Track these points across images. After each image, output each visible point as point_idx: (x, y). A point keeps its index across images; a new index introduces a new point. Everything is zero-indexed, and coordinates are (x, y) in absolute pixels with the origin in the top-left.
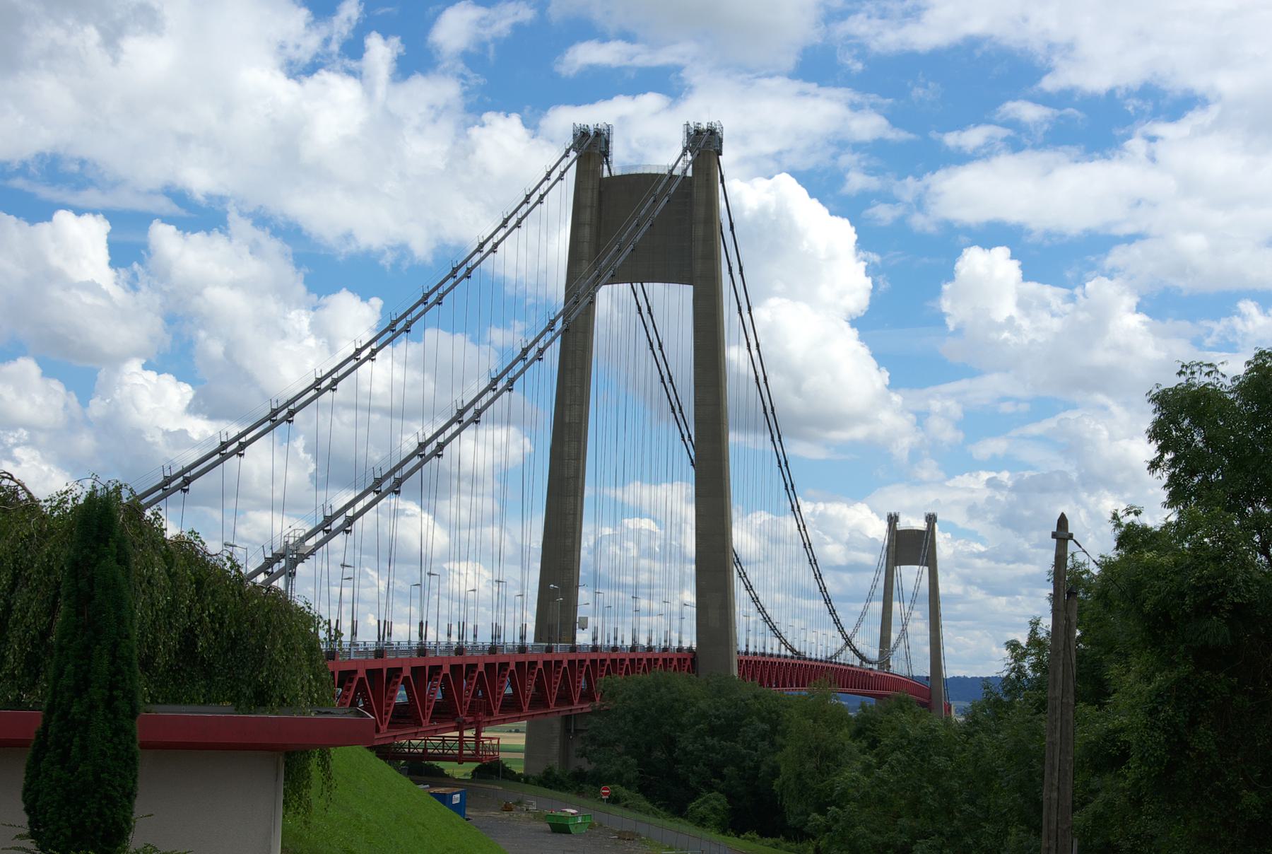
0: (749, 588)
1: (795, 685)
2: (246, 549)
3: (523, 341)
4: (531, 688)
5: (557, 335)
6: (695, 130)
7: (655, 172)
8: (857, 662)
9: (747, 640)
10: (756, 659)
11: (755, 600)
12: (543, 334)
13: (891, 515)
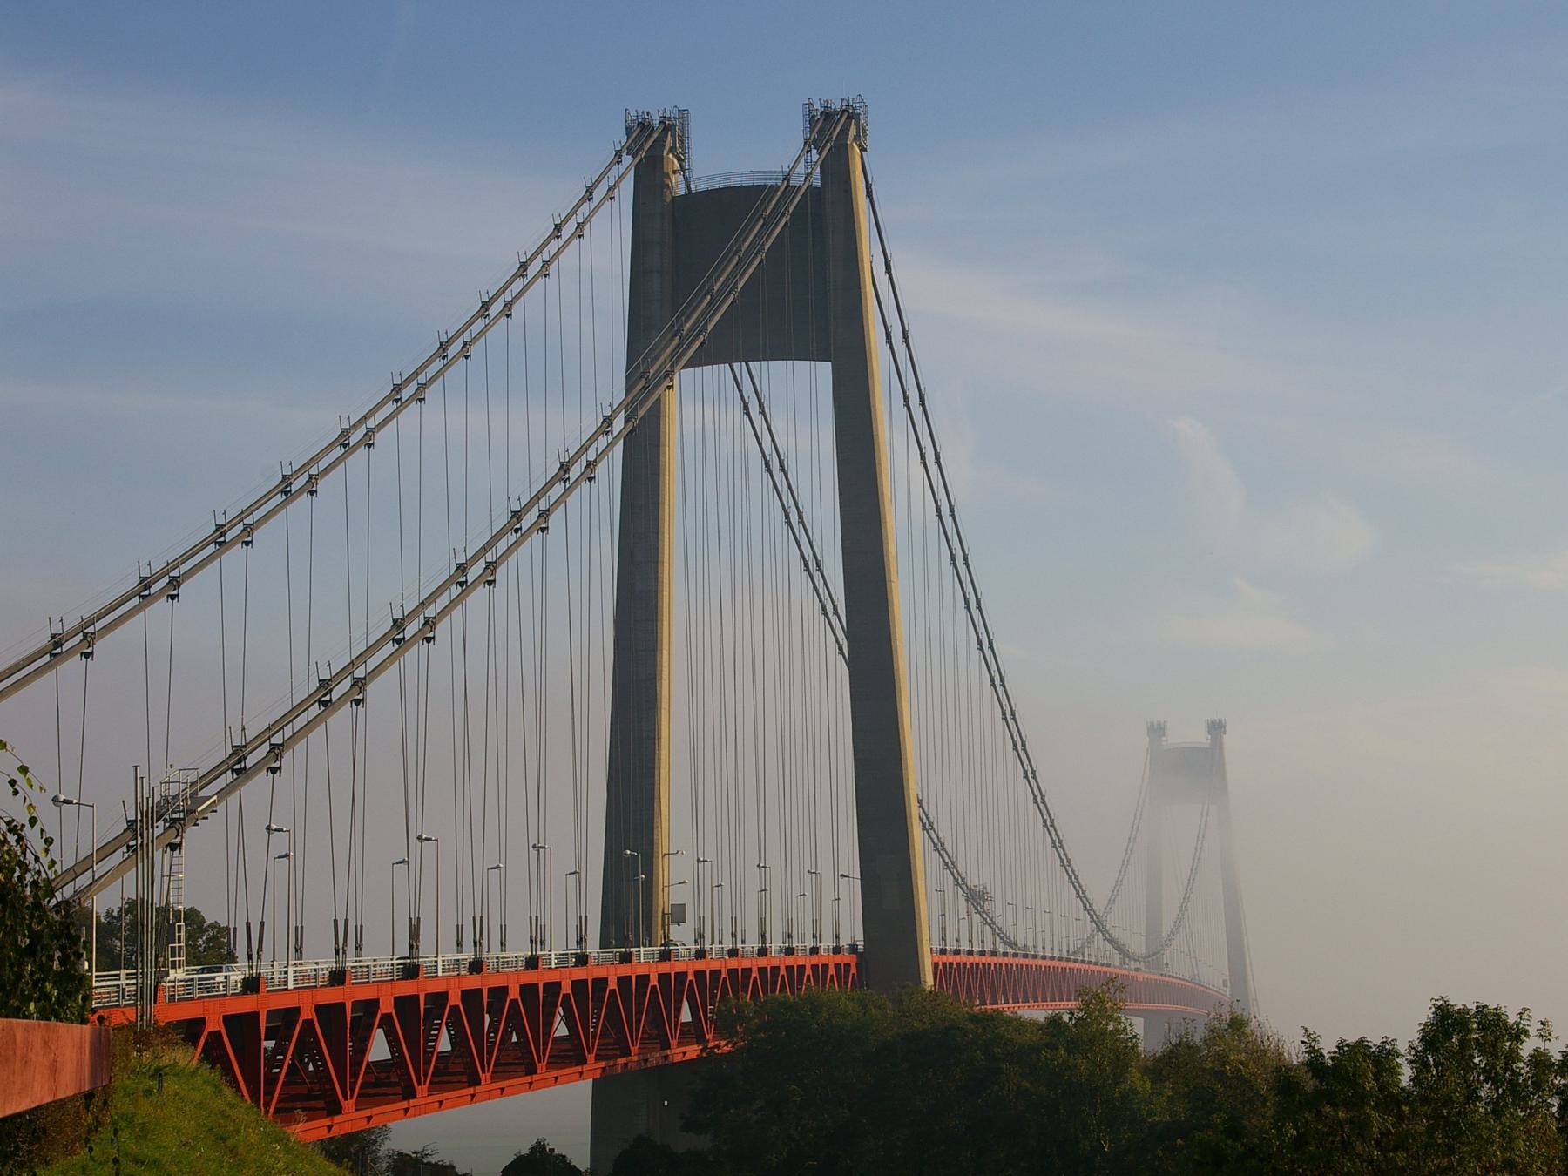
0: (939, 847)
1: (1011, 1001)
2: (93, 806)
3: (562, 451)
4: (598, 1024)
5: (616, 439)
6: (822, 113)
7: (762, 183)
8: (1116, 959)
9: (958, 931)
10: (984, 961)
11: (950, 866)
12: (593, 438)
13: (1152, 724)
